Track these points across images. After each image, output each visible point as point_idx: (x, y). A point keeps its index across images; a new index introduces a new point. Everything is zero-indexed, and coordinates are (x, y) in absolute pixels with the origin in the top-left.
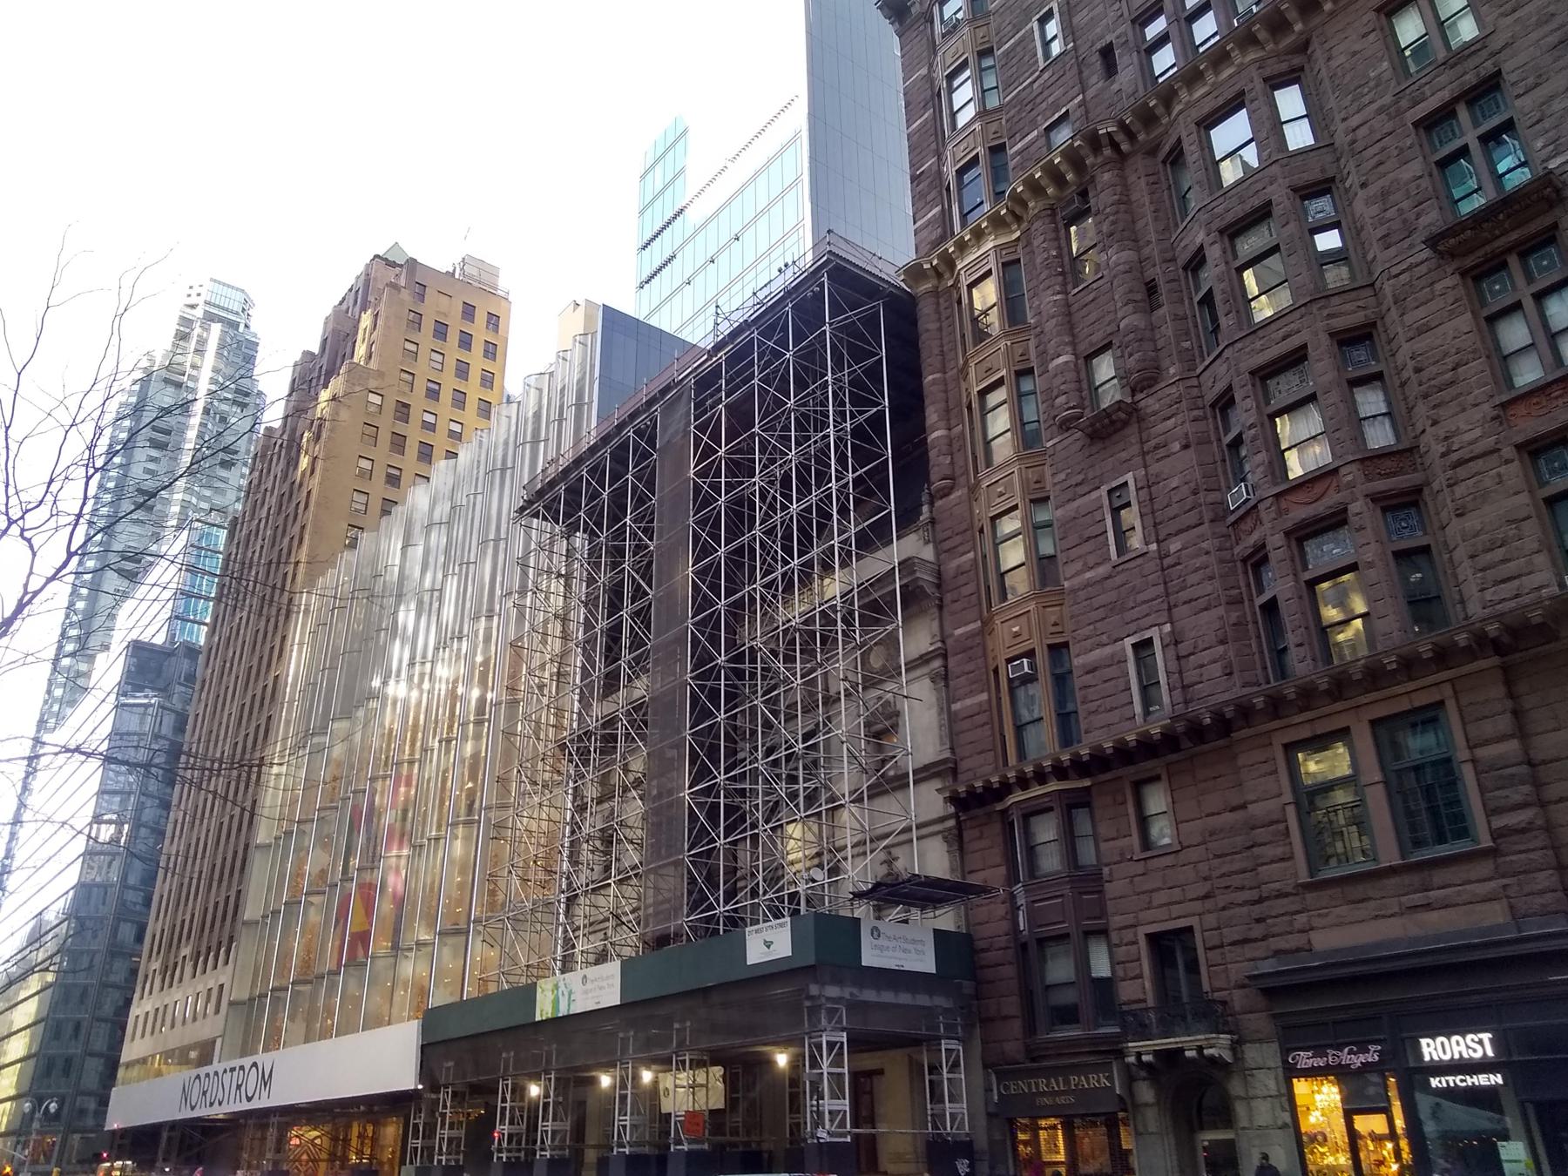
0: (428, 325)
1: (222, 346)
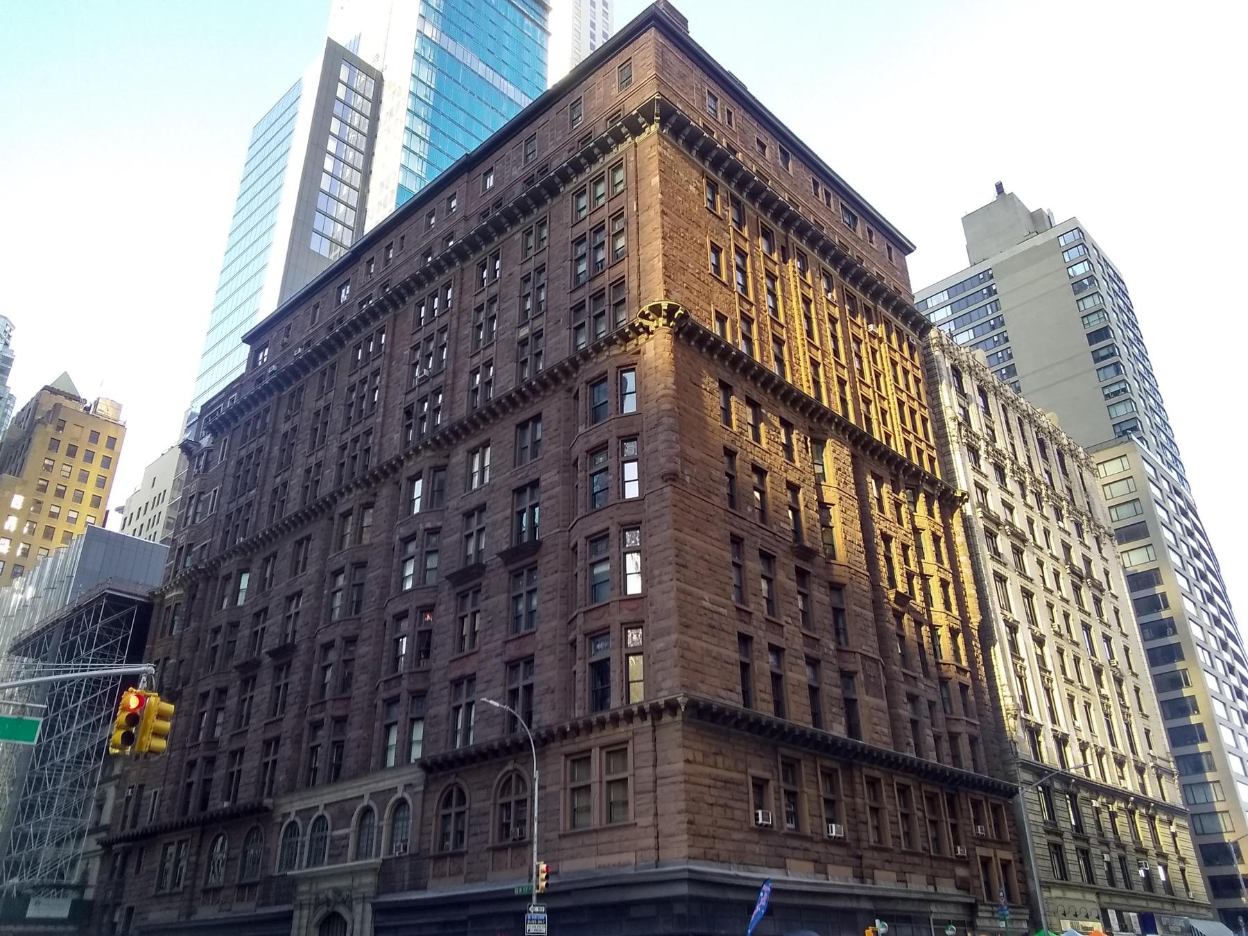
0: (63, 447)
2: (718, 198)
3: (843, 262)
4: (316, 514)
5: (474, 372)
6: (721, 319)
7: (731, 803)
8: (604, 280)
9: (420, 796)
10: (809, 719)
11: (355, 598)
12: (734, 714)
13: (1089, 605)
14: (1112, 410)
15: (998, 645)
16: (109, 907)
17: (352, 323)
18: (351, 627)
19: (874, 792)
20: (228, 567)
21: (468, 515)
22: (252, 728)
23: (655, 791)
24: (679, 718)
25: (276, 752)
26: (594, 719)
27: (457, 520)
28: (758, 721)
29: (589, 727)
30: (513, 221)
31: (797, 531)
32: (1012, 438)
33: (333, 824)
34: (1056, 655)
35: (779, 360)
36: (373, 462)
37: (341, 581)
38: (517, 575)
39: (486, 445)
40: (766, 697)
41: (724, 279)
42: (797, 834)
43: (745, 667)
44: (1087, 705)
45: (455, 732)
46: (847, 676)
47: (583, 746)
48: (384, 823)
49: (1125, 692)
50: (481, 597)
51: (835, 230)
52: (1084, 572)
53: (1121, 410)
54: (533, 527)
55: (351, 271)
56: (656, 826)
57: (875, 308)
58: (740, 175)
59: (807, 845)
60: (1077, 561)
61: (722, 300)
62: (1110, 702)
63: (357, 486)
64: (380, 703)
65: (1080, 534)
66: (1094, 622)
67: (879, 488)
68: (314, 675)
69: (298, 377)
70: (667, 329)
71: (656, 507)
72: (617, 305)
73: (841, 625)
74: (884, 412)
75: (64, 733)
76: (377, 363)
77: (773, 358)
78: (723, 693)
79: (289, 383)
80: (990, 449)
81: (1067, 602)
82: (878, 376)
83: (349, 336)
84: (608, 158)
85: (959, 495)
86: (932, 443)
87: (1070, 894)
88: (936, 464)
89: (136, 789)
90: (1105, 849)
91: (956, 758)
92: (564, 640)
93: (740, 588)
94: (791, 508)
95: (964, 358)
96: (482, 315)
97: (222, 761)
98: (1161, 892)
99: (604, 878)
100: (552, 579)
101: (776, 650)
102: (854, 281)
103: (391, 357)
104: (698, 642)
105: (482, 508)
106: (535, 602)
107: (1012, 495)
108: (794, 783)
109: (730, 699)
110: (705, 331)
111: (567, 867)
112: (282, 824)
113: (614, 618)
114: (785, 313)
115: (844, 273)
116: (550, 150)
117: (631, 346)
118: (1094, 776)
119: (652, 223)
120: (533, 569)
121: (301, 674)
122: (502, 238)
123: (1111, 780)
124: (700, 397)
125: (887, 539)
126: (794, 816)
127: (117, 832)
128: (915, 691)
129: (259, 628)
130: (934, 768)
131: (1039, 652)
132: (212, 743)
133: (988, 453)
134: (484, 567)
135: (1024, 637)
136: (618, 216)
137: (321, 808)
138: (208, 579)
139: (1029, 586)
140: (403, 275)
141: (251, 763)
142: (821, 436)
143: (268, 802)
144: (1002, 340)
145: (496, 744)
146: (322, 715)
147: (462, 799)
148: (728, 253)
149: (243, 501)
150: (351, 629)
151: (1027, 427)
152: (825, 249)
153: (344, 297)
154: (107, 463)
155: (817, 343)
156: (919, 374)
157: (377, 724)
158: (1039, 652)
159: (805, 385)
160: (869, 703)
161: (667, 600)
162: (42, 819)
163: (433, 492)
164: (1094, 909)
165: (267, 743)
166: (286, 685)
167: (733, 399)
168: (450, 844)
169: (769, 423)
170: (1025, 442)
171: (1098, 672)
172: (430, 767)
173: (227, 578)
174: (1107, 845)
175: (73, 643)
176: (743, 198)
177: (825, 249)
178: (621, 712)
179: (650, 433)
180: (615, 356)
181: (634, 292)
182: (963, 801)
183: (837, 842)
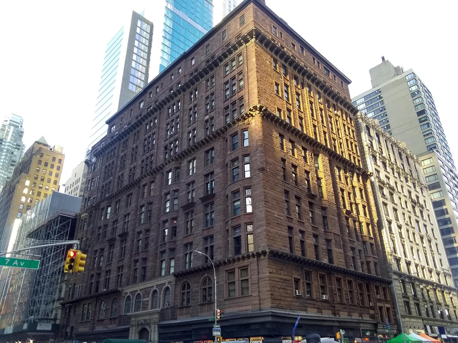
0: (43, 163)
1: (13, 132)
2: (277, 65)
3: (325, 88)
4: (134, 185)
5: (189, 133)
6: (279, 110)
7: (286, 288)
8: (236, 97)
9: (174, 286)
10: (315, 257)
12: (287, 255)
13: (418, 213)
15: (384, 229)
17: (145, 116)
21: (188, 185)
23: (258, 284)
24: (267, 257)
25: (122, 271)
26: (236, 258)
27: (184, 187)
29: (234, 261)
30: (202, 76)
31: (309, 188)
32: (389, 152)
33: (143, 296)
35: (301, 125)
36: (154, 166)
37: (144, 209)
38: (206, 206)
39: (194, 159)
40: (299, 249)
41: (280, 95)
42: (311, 299)
43: (290, 238)
44: (418, 250)
45: (186, 263)
46: (328, 241)
47: (232, 267)
49: (432, 245)
50: (194, 214)
51: (321, 76)
52: (416, 201)
53: (430, 141)
54: (212, 189)
56: (259, 296)
58: (285, 56)
59: (315, 302)
60: (414, 197)
64: (159, 253)
66: (420, 219)
67: (339, 172)
70: (260, 115)
71: (257, 181)
73: (326, 222)
74: (341, 143)
77: (299, 124)
78: (283, 248)
79: (123, 138)
80: (381, 156)
81: (410, 212)
82: (338, 130)
83: (144, 121)
84: (237, 52)
85: (369, 173)
86: (359, 154)
87: (412, 320)
88: (360, 162)
89: (73, 284)
90: (426, 303)
91: (369, 270)
92: (224, 229)
93: (288, 209)
94: (306, 180)
95: (370, 123)
96: (192, 111)
97: (103, 274)
98: (447, 319)
100: (219, 207)
101: (302, 232)
102: (329, 95)
103: (159, 128)
104: (273, 230)
105: (193, 182)
106: (213, 216)
107: (389, 173)
108: (309, 280)
110: (273, 115)
111: (227, 311)
112: (125, 296)
113: (242, 221)
116: (215, 49)
117: (246, 121)
118: (421, 276)
120: (212, 204)
121: (130, 243)
122: (198, 83)
123: (427, 277)
124: (272, 140)
125: (342, 190)
126: (309, 292)
127: (67, 300)
128: (354, 246)
129: (115, 226)
130: (361, 274)
131: (400, 231)
132: (99, 268)
133: (380, 158)
135: (394, 226)
136: (240, 73)
137: (139, 291)
138: (96, 209)
139: (396, 207)
140: (163, 98)
141: (113, 275)
142: (317, 153)
143: (120, 289)
144: (385, 116)
145: (201, 267)
146: (138, 257)
147: (189, 287)
148: (281, 86)
149: (108, 181)
150: (147, 226)
151: (394, 148)
153: (141, 106)
154: (59, 168)
156: (354, 129)
158: (400, 231)
159: (311, 134)
160: (337, 251)
161: (261, 215)
164: (422, 325)
165: (119, 268)
166: (125, 247)
168: (185, 303)
169: (298, 149)
170: (394, 154)
171: (422, 238)
172: (177, 276)
173: (103, 209)
176: (287, 65)
178: (246, 255)
179: (254, 153)
180: (241, 125)
181: (247, 101)
182: (372, 286)
183: (325, 301)
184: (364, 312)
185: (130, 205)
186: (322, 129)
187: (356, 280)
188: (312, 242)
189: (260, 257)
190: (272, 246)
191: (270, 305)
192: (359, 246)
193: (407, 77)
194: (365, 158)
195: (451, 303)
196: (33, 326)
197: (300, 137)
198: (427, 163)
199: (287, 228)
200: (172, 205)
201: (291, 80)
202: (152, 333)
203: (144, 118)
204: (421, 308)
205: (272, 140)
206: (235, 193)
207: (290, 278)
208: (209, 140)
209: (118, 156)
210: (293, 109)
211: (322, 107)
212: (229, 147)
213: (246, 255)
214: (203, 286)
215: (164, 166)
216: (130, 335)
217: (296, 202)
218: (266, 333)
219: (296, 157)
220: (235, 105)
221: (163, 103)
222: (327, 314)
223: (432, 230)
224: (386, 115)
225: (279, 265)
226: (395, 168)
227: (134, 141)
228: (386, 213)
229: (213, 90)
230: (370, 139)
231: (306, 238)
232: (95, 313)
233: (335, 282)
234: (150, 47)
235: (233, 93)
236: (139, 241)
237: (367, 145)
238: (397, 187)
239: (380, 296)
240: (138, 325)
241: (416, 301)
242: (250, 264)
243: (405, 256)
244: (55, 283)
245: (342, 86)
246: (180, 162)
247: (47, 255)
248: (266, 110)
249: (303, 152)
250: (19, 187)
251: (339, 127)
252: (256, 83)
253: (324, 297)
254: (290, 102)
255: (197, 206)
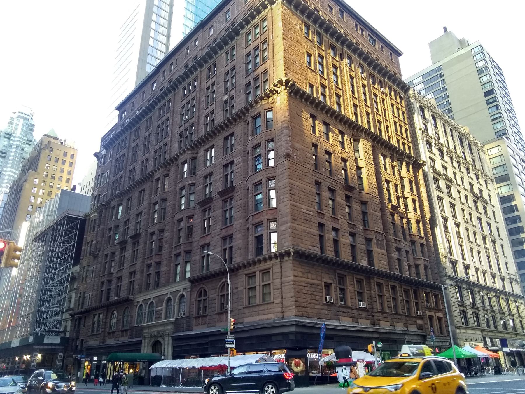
0: (53, 159)
1: (23, 126)
2: (310, 32)
3: (369, 60)
4: (146, 180)
5: (207, 116)
6: (311, 86)
7: (315, 293)
8: (259, 71)
9: (189, 293)
10: (351, 258)
11: (163, 214)
12: (315, 256)
13: (481, 209)
14: (495, 126)
15: (438, 227)
16: (75, 340)
17: (157, 98)
18: (161, 226)
19: (380, 289)
20: (114, 203)
21: (206, 177)
22: (125, 267)
23: (281, 289)
24: (291, 258)
25: (134, 277)
26: (256, 260)
27: (201, 180)
28: (326, 259)
29: (254, 263)
30: (221, 48)
31: (346, 179)
32: (447, 138)
33: (157, 305)
34: (465, 231)
35: (339, 104)
36: (168, 157)
37: (157, 207)
38: (225, 201)
39: (212, 147)
40: (331, 249)
41: (313, 68)
42: (345, 306)
43: (321, 237)
44: (479, 252)
45: (203, 267)
46: (368, 241)
47: (252, 271)
48: (176, 304)
49: (496, 247)
50: (211, 211)
51: (366, 46)
52: (479, 195)
53: (499, 126)
54: (232, 182)
55: (157, 76)
56: (282, 303)
57: (384, 81)
58: (320, 21)
59: (349, 311)
60: (476, 191)
61: (312, 78)
62: (490, 251)
63: (162, 167)
64: (173, 256)
65: (460, 168)
66: (483, 217)
67: (385, 160)
68: (147, 245)
69: (137, 123)
70: (286, 91)
71: (282, 170)
72: (265, 82)
73: (366, 219)
74: (387, 127)
75: (54, 272)
76: (168, 115)
77: (335, 103)
78: (311, 248)
79: (134, 126)
80: (437, 142)
81: (471, 208)
82: (385, 111)
83: (157, 104)
84: (260, 16)
85: (421, 162)
86: (410, 140)
87: (469, 331)
88: (411, 149)
89: (82, 293)
90: (486, 312)
91: (418, 274)
92: (245, 228)
93: (319, 204)
94: (343, 169)
95: (425, 103)
96: (209, 91)
97: (114, 281)
98: (511, 330)
99: (261, 325)
100: (240, 202)
101: (336, 230)
102: (374, 68)
103: (173, 111)
104: (300, 226)
105: (211, 174)
106: (233, 213)
107: (447, 162)
108: (344, 285)
109: (315, 250)
110: (303, 91)
111: (247, 320)
112: (137, 305)
113: (264, 218)
114: (342, 83)
115: (369, 65)
116: (236, 15)
117: (270, 100)
118: (482, 282)
119: (279, 43)
120: (232, 198)
121: (143, 245)
122: (217, 56)
123: (489, 283)
124: (301, 121)
125: (388, 182)
126: (343, 299)
127: (76, 310)
128: (400, 247)
129: (126, 227)
130: (408, 278)
131: (457, 230)
132: (110, 274)
133: (436, 144)
134: (212, 199)
135: (451, 223)
136: (264, 42)
137: (152, 299)
138: (106, 209)
139: (453, 202)
140: (177, 76)
141: (125, 282)
142: (357, 138)
143: (131, 297)
144: (446, 97)
145: (218, 271)
146: (151, 261)
147: (206, 294)
148: (314, 56)
149: (118, 176)
150: (161, 226)
151: (454, 133)
152: (361, 55)
153: (154, 88)
154: (71, 164)
155: (326, 77)
156: (404, 110)
157: (172, 264)
158: (457, 230)
159: (351, 115)
160: (378, 252)
161: (286, 209)
162: (47, 306)
163: (192, 168)
164: (480, 337)
165: (131, 274)
166: (137, 250)
167: (317, 122)
168: (201, 312)
169: (333, 132)
170: (453, 140)
171: (484, 238)
172: (193, 281)
173: (113, 208)
174: (487, 311)
175: (55, 236)
176: (322, 32)
177: (361, 55)
178: (267, 256)
179: (279, 138)
180: (264, 104)
181: (272, 75)
182: (420, 292)
183: (363, 309)
184: (410, 322)
185: (143, 203)
186: (364, 110)
187: (401, 285)
188: (348, 242)
189: (283, 258)
190: (298, 245)
191: (294, 313)
192: (406, 246)
193: (473, 50)
194: (418, 144)
195: (517, 313)
196: (39, 339)
197: (336, 118)
198: (495, 151)
199: (317, 225)
200: (188, 202)
201: (326, 50)
202: (166, 346)
203: (156, 101)
204: (481, 318)
205: (301, 122)
206: (257, 184)
207: (319, 282)
208: (228, 124)
209: (129, 146)
210: (329, 85)
211: (366, 83)
212: (250, 132)
213: (267, 256)
214: (221, 292)
215: (178, 156)
216: (143, 348)
217: (330, 195)
218: (288, 345)
219: (331, 142)
220: (256, 81)
221: (177, 83)
222: (364, 324)
223: (498, 229)
224: (448, 97)
225: (307, 268)
226: (454, 157)
227: (147, 129)
228: (441, 208)
229: (233, 63)
230: (424, 122)
231: (341, 236)
232: (105, 325)
233: (374, 287)
234: (170, 21)
235: (256, 65)
236: (152, 242)
237: (420, 129)
238: (456, 179)
239: (431, 304)
240: (151, 337)
241: (474, 310)
242: (272, 267)
243: (463, 259)
244: (64, 291)
245: (391, 58)
246: (196, 151)
247: (54, 261)
248: (293, 85)
249: (340, 136)
250: (27, 186)
251: (386, 107)
252: (282, 52)
253: (361, 304)
254: (326, 77)
255: (215, 202)
